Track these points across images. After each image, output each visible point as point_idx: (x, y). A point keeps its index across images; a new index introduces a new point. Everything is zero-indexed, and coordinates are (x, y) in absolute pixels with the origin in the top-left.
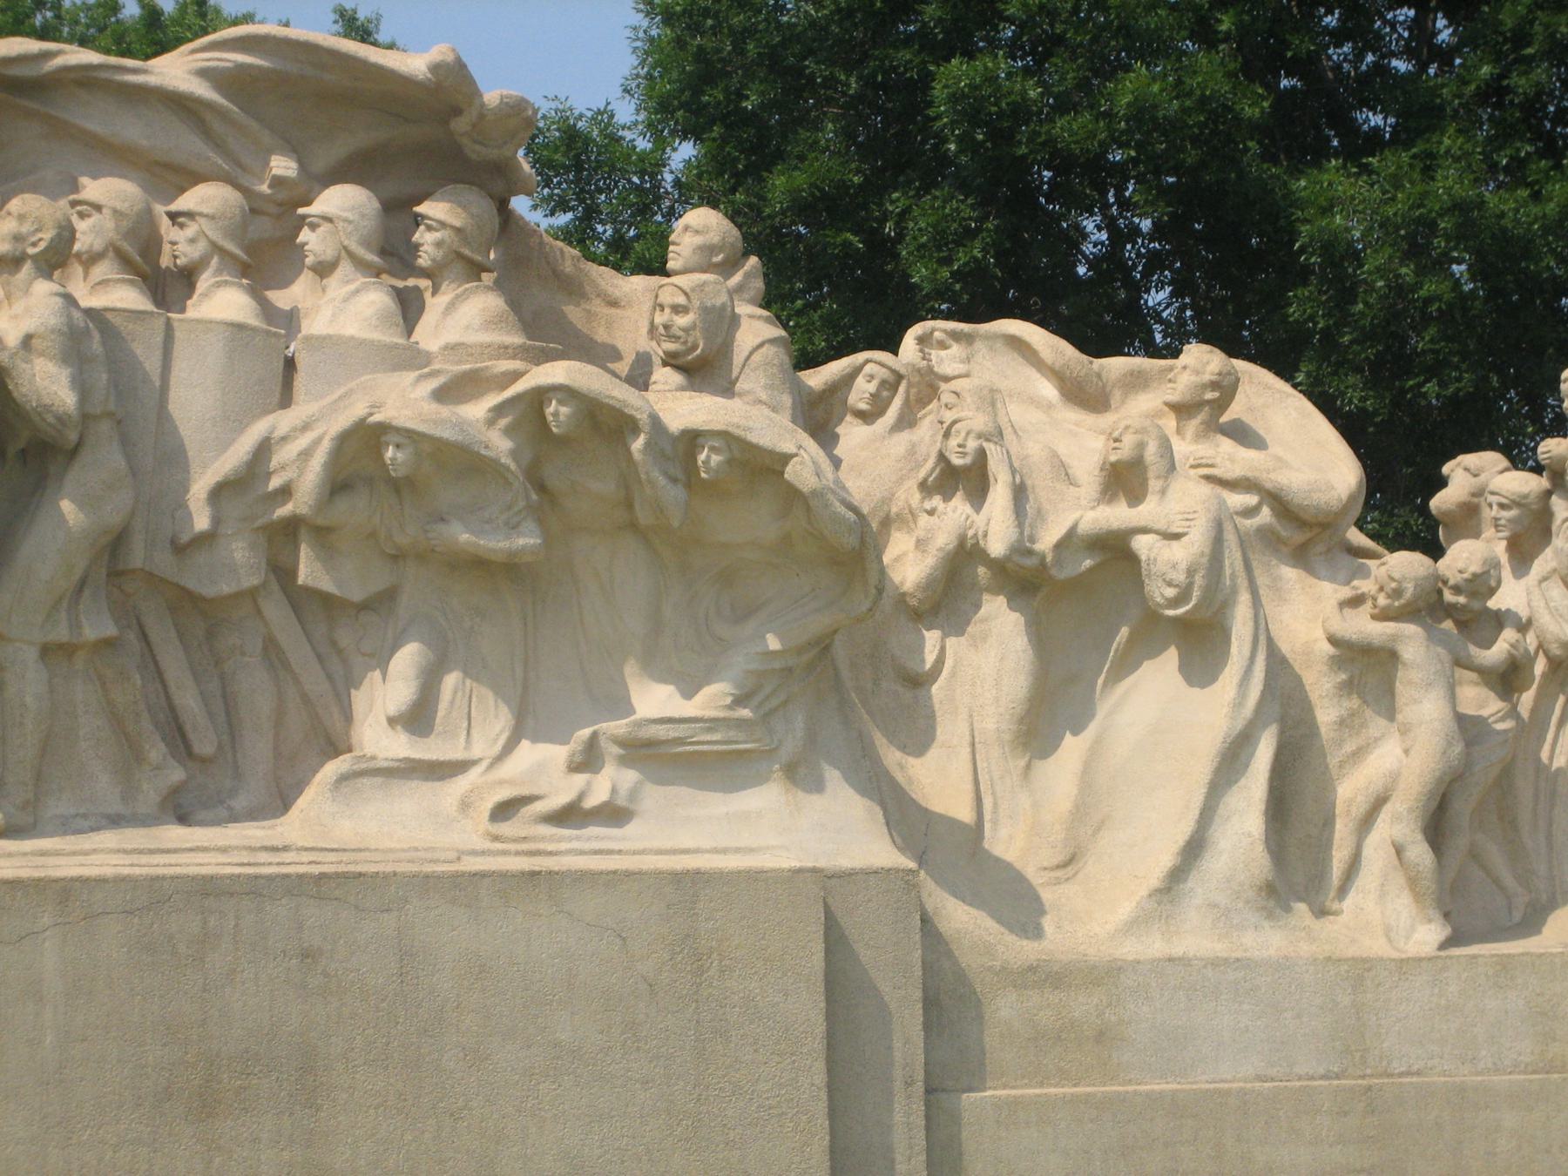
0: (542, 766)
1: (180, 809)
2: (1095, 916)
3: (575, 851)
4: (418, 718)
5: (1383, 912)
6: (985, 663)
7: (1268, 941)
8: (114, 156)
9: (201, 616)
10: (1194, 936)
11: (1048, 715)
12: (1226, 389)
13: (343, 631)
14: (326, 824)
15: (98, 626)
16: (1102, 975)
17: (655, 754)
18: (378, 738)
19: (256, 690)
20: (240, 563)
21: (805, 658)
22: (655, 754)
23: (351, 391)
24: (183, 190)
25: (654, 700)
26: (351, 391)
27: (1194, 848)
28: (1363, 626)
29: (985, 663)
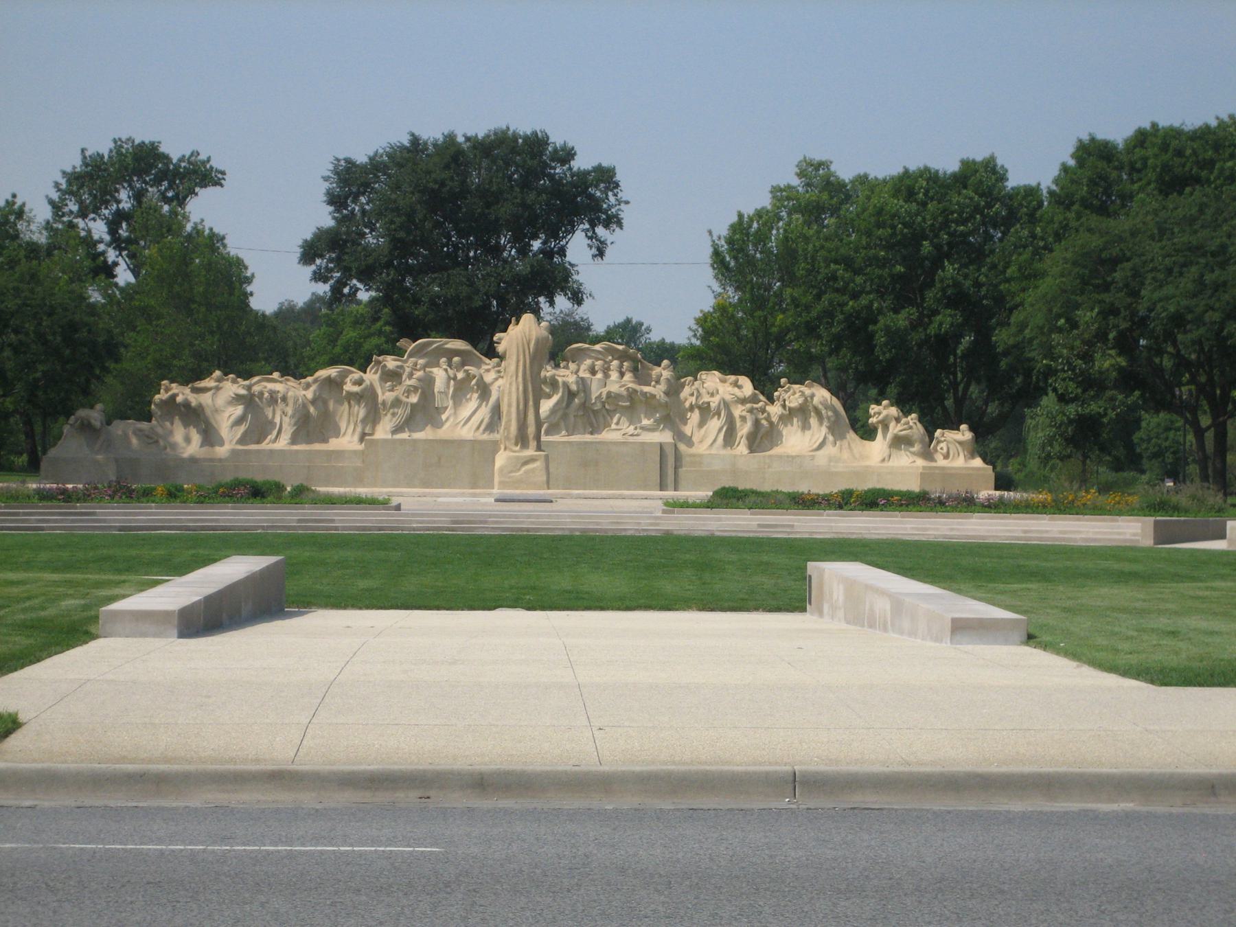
0: (631, 429)
1: (592, 433)
2: (701, 449)
3: (631, 439)
4: (617, 423)
5: (742, 448)
6: (695, 417)
7: (723, 452)
8: (590, 357)
9: (595, 412)
10: (714, 451)
11: (702, 423)
12: (737, 381)
13: (611, 413)
14: (607, 436)
15: (581, 413)
16: (701, 456)
17: (642, 428)
18: (613, 426)
19: (601, 419)
20: (598, 406)
21: (559, 414)
22: (642, 428)
23: (124, 582)
24: (494, 461)
25: (645, 422)
26: (124, 582)
27: (715, 441)
28: (744, 413)
29: (695, 417)
